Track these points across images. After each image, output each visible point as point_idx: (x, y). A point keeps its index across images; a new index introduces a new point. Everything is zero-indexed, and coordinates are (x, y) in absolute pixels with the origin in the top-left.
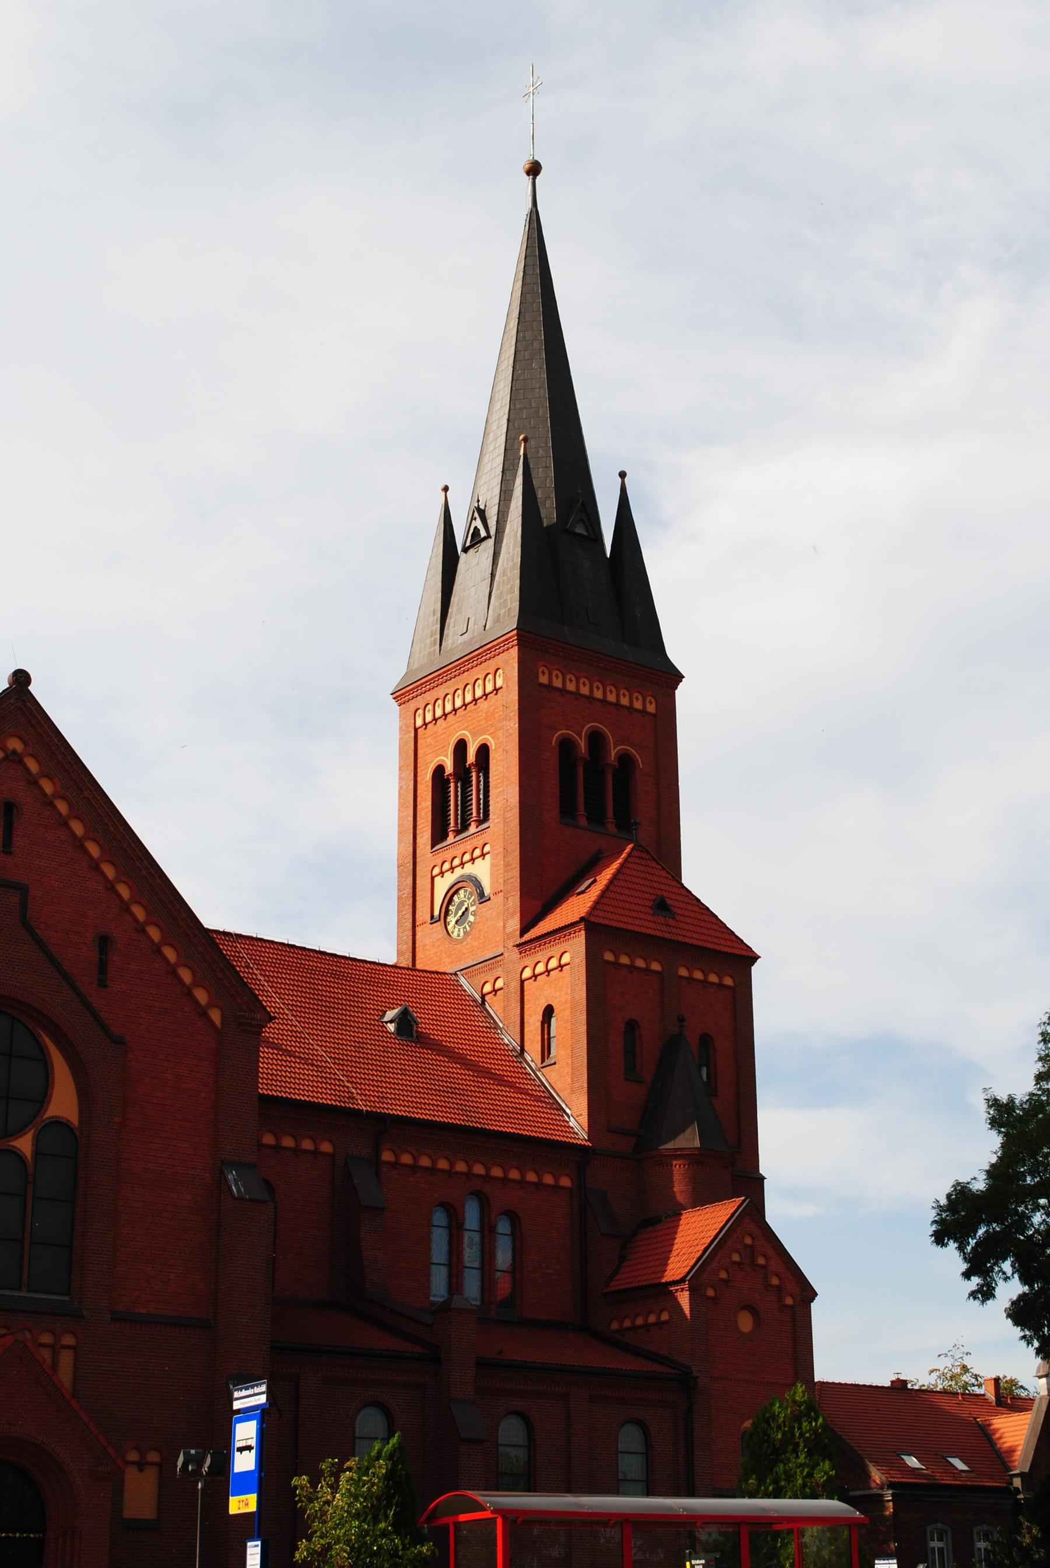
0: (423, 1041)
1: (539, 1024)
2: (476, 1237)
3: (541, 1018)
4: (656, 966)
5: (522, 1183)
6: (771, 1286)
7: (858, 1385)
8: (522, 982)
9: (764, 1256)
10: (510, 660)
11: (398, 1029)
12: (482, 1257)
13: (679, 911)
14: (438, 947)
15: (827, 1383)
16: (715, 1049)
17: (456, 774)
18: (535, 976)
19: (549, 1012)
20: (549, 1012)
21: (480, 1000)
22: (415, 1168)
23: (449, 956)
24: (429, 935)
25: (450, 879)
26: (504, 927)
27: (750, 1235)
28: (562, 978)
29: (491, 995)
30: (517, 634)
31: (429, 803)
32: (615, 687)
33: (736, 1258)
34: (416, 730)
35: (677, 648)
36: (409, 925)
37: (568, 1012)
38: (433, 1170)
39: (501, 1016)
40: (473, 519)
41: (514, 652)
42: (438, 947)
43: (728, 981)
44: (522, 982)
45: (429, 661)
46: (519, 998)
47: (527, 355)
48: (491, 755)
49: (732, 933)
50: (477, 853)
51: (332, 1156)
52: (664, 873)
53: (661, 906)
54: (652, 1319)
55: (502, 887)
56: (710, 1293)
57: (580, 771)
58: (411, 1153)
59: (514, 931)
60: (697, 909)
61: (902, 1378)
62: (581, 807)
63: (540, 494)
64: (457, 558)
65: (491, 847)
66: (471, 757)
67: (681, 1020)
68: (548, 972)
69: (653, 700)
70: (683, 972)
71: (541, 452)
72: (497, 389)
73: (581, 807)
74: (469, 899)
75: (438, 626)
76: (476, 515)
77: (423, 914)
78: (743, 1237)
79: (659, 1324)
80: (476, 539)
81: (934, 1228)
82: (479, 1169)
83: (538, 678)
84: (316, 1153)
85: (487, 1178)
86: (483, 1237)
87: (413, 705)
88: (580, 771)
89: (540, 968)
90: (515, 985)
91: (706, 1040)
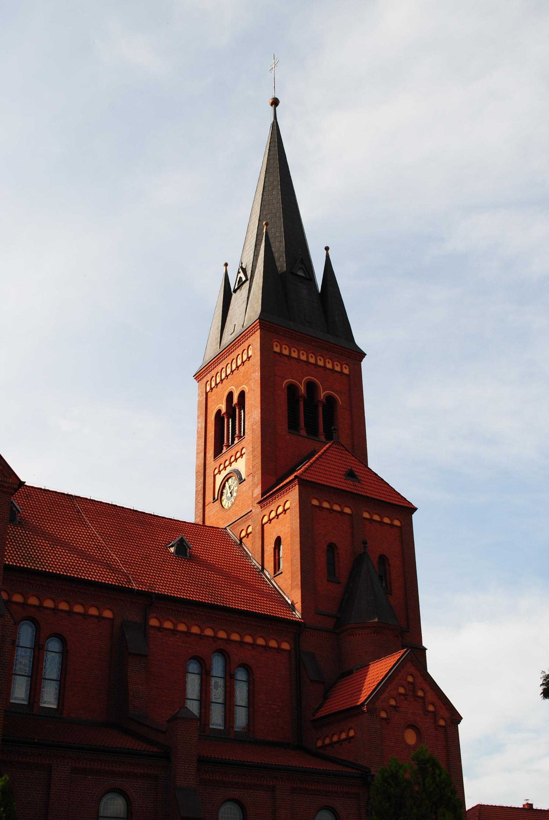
0: (192, 558)
1: (272, 550)
2: (221, 682)
3: (273, 546)
4: (347, 510)
5: (254, 645)
6: (429, 712)
7: (503, 807)
8: (263, 526)
9: (422, 690)
10: (255, 340)
11: (177, 551)
12: (225, 696)
13: (363, 479)
14: (217, 515)
15: (484, 805)
16: (389, 565)
17: (227, 412)
18: (270, 520)
19: (278, 541)
20: (278, 541)
21: (260, 567)
22: (174, 631)
23: (223, 520)
24: (212, 509)
25: (224, 473)
26: (253, 494)
27: (412, 675)
28: (285, 518)
29: (245, 538)
30: (259, 322)
31: (213, 433)
32: (323, 357)
33: (402, 690)
34: (207, 393)
35: (361, 338)
36: (201, 506)
37: (289, 539)
38: (188, 634)
39: (250, 547)
40: (239, 273)
41: (258, 333)
42: (217, 515)
43: (397, 523)
44: (263, 526)
45: (213, 350)
46: (260, 536)
47: (270, 188)
48: (246, 396)
49: (399, 494)
50: (238, 455)
51: (112, 620)
52: (353, 458)
53: (351, 474)
54: (343, 736)
55: (251, 472)
56: (383, 715)
57: (301, 404)
58: (172, 621)
59: (258, 495)
60: (375, 479)
61: (530, 802)
62: (302, 424)
63: (276, 255)
64: (232, 295)
65: (246, 449)
66: (235, 400)
67: (365, 543)
68: (277, 516)
69: (347, 367)
70: (366, 515)
71: (277, 234)
72: (254, 209)
73: (302, 424)
74: (234, 483)
75: (220, 334)
76: (240, 270)
77: (209, 498)
78: (407, 676)
79: (348, 739)
80: (241, 283)
81: (543, 687)
82: (222, 635)
83: (273, 347)
84: (100, 618)
85: (228, 641)
86: (225, 683)
87: (205, 380)
88: (301, 404)
89: (273, 515)
90: (259, 528)
91: (383, 559)
